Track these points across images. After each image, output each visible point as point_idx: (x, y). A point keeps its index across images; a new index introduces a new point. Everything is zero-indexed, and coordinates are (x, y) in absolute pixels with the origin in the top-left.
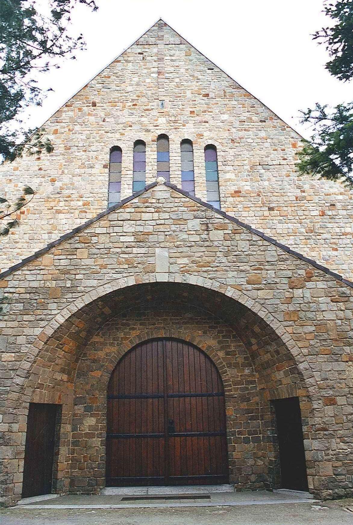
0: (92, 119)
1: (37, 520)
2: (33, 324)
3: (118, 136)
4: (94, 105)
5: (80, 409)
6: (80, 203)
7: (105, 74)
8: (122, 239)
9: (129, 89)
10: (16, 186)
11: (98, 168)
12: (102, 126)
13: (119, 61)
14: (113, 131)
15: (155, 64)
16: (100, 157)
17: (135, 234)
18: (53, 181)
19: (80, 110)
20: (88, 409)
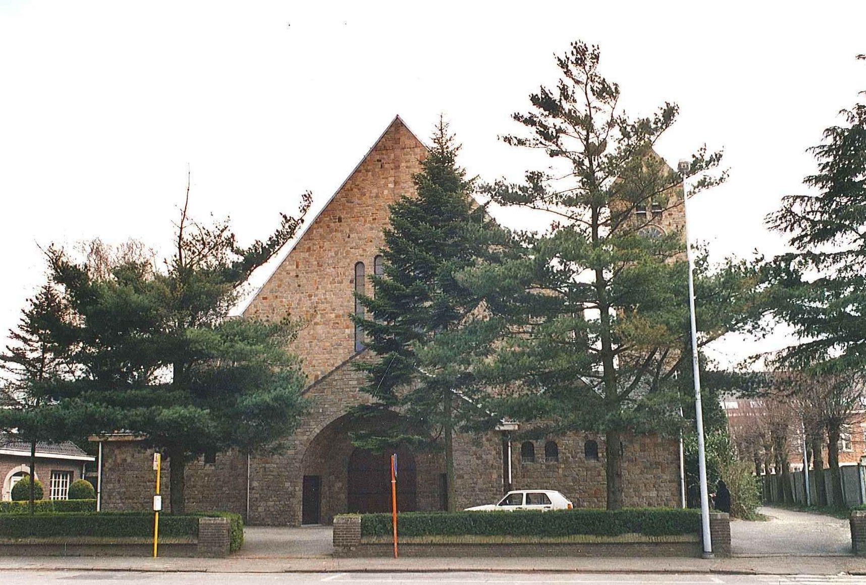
0: (339, 235)
1: (744, 254)
2: (303, 434)
3: (361, 252)
4: (340, 220)
5: (332, 478)
6: (333, 316)
7: (348, 186)
8: (351, 383)
9: (369, 202)
10: (281, 302)
11: (346, 283)
12: (347, 243)
13: (360, 171)
14: (357, 247)
15: (392, 172)
16: (347, 274)
17: (358, 379)
18: (310, 296)
19: (328, 226)
20: (337, 477)
